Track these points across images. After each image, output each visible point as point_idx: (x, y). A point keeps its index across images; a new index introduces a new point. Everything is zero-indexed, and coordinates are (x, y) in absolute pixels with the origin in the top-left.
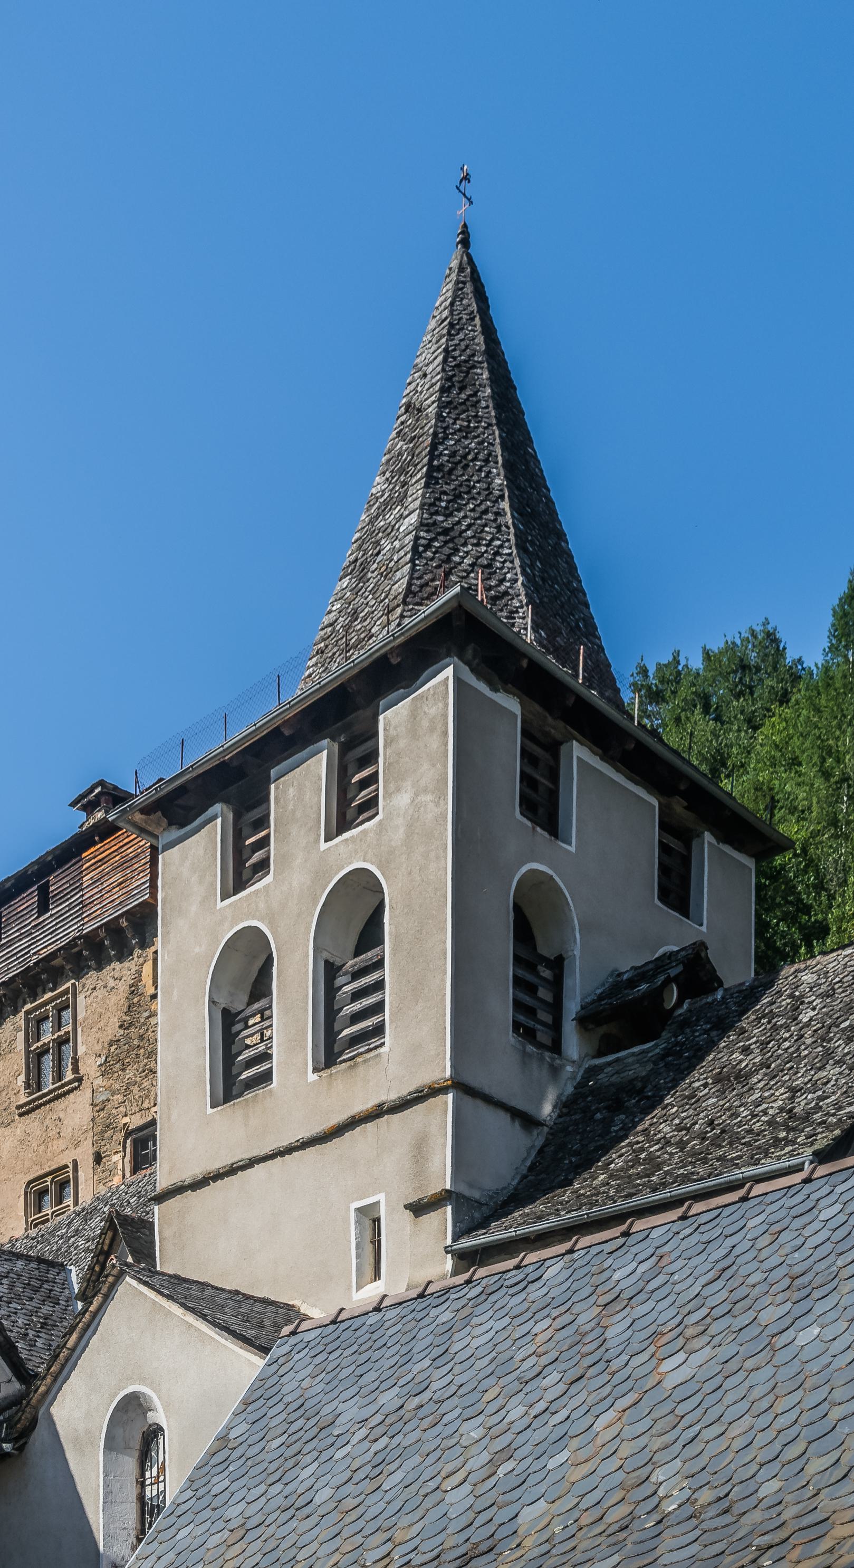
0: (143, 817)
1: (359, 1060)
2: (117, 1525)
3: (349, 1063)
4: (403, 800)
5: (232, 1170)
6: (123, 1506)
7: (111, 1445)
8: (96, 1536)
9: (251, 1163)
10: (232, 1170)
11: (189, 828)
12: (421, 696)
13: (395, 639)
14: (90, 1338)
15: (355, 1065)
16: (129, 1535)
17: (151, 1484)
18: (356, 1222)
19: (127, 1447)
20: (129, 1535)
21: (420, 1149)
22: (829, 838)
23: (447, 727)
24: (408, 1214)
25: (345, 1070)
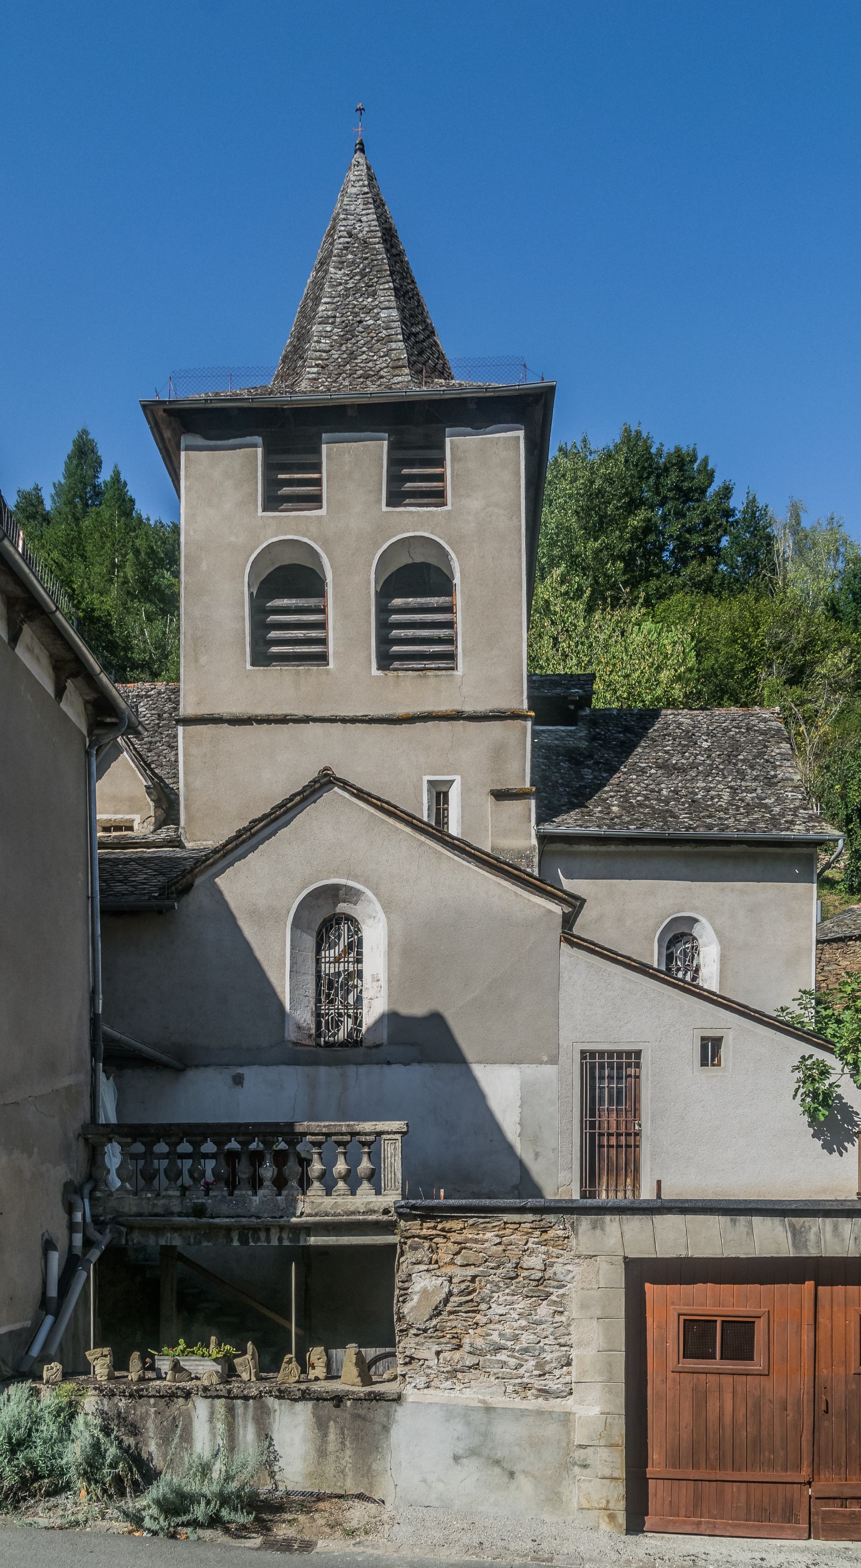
0: (165, 415)
1: (429, 673)
2: (301, 992)
3: (420, 673)
4: (475, 503)
5: (284, 720)
6: (305, 977)
7: (296, 924)
8: (281, 996)
9: (306, 720)
10: (284, 720)
11: (213, 443)
12: (492, 440)
13: (486, 391)
14: (280, 828)
15: (425, 676)
16: (309, 1002)
17: (325, 963)
18: (428, 790)
19: (309, 928)
20: (309, 1002)
21: (498, 752)
22: (125, 577)
23: (519, 468)
24: (491, 798)
25: (413, 677)
